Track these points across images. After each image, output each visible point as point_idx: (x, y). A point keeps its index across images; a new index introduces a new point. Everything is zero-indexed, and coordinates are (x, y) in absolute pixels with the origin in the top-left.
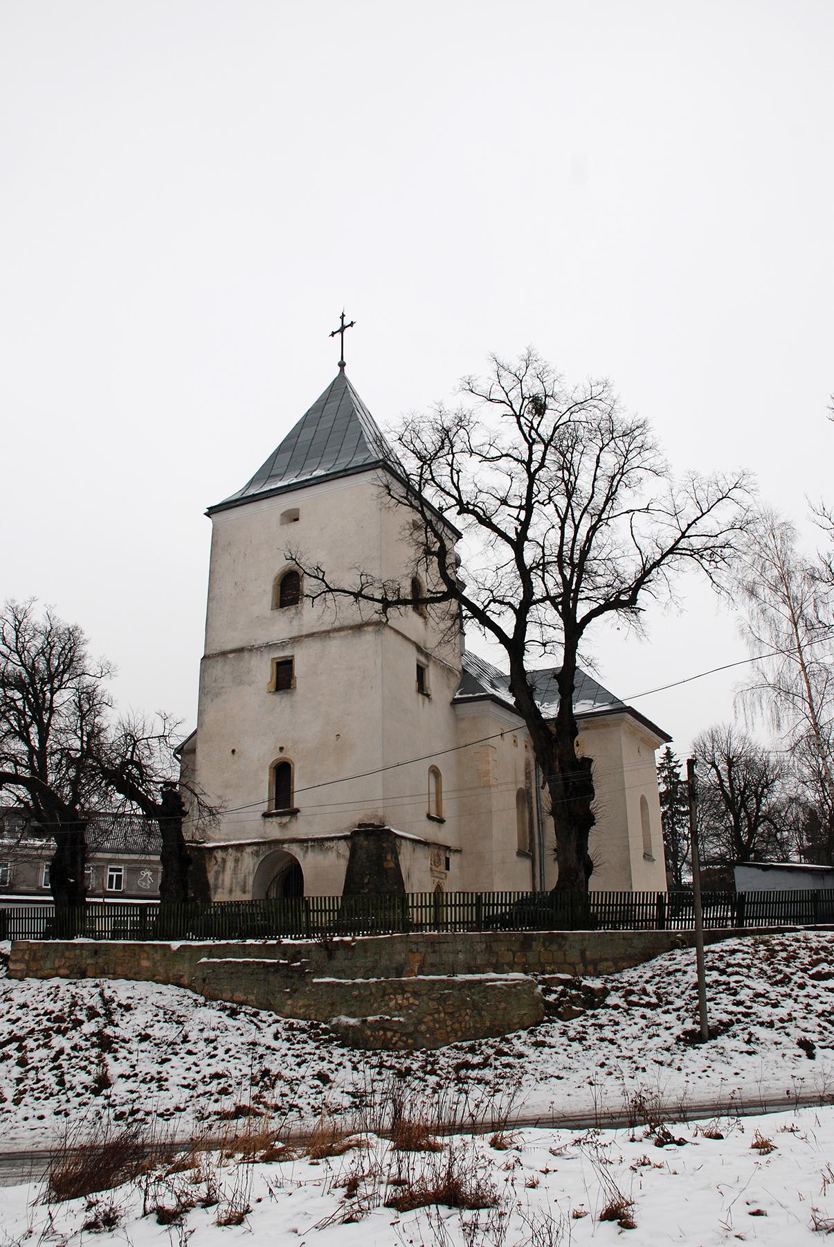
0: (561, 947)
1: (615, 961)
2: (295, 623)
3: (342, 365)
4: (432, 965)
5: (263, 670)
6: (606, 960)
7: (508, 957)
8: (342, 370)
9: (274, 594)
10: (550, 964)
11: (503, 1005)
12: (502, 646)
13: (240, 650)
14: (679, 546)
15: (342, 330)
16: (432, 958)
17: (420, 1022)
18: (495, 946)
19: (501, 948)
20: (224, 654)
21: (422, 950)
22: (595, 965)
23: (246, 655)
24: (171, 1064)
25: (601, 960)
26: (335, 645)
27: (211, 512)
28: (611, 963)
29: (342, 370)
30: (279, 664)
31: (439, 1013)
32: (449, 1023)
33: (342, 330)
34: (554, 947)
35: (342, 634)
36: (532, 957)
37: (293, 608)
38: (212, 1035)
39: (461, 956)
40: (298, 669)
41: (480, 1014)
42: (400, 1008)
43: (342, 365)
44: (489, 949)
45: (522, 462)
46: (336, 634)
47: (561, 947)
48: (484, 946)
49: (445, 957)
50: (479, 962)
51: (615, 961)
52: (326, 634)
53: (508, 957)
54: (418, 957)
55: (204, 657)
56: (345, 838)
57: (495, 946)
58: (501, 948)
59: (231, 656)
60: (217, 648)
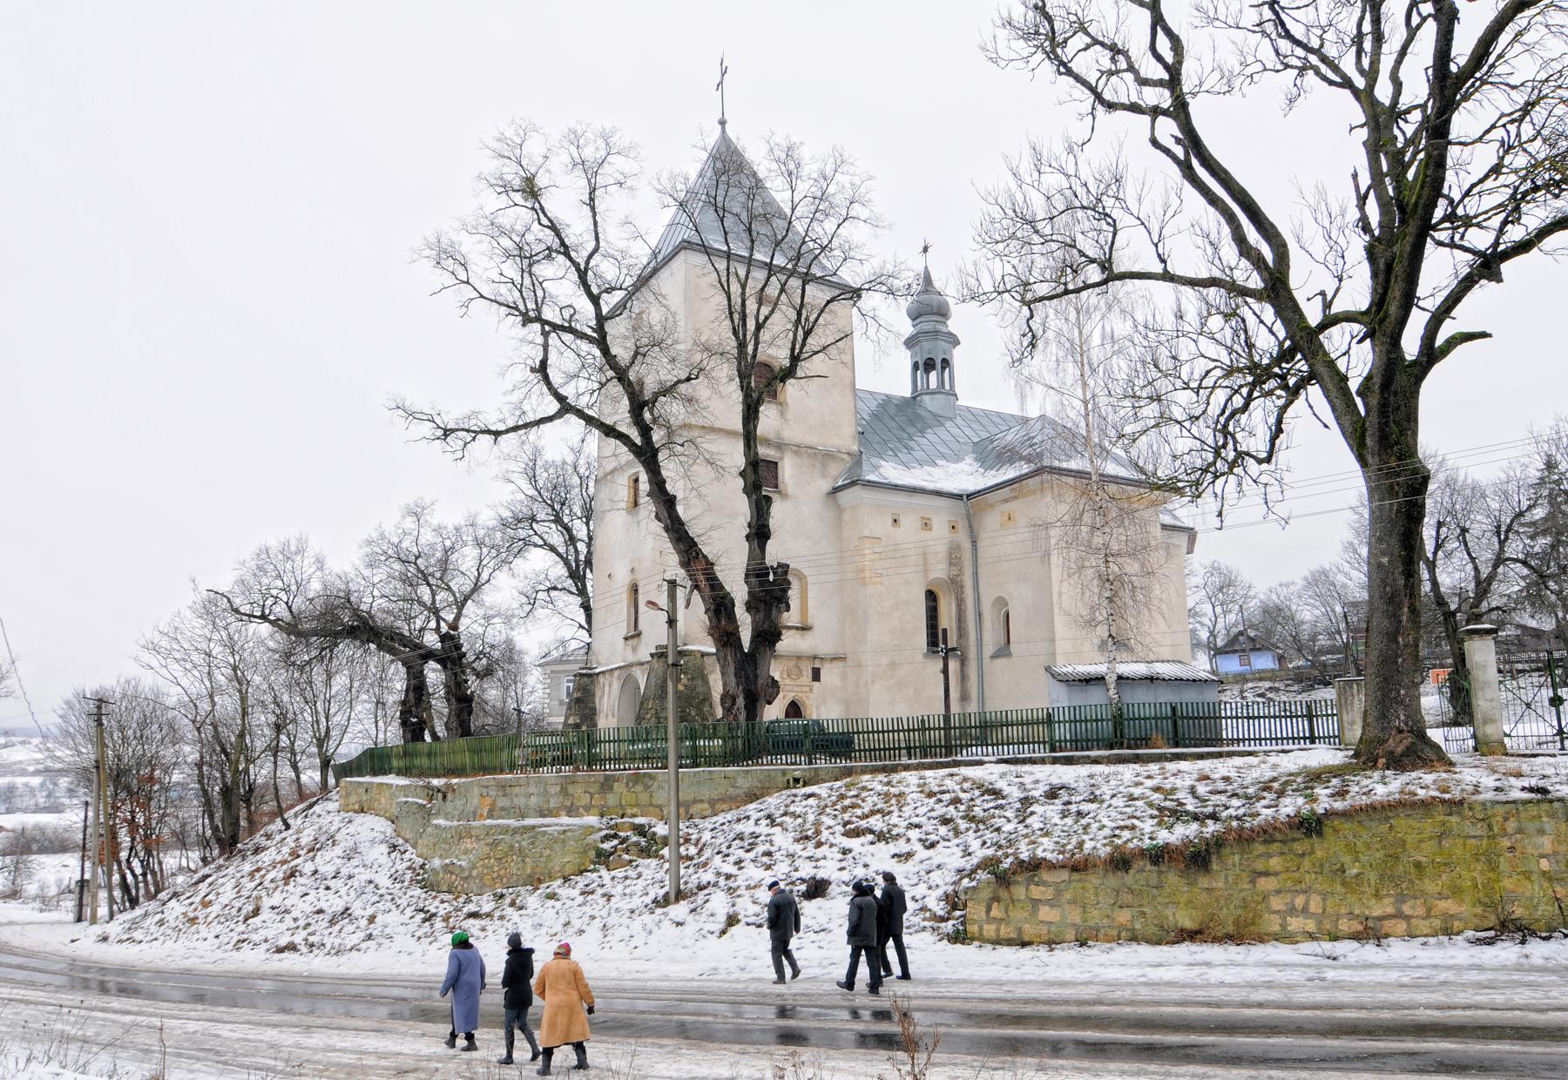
0: (647, 787)
1: (712, 803)
3: (723, 123)
4: (502, 809)
6: (702, 801)
7: (586, 799)
8: (724, 131)
10: (632, 806)
11: (547, 852)
14: (429, 603)
16: (502, 802)
17: (474, 867)
18: (571, 789)
19: (577, 790)
21: (493, 793)
22: (687, 808)
24: (829, 937)
25: (695, 802)
28: (706, 805)
29: (724, 131)
34: (639, 788)
36: (612, 799)
39: (533, 799)
42: (466, 852)
43: (723, 123)
44: (564, 791)
45: (1087, 47)
47: (647, 787)
48: (558, 788)
49: (516, 800)
50: (552, 805)
51: (712, 803)
53: (586, 799)
54: (488, 801)
57: (571, 789)
58: (577, 790)
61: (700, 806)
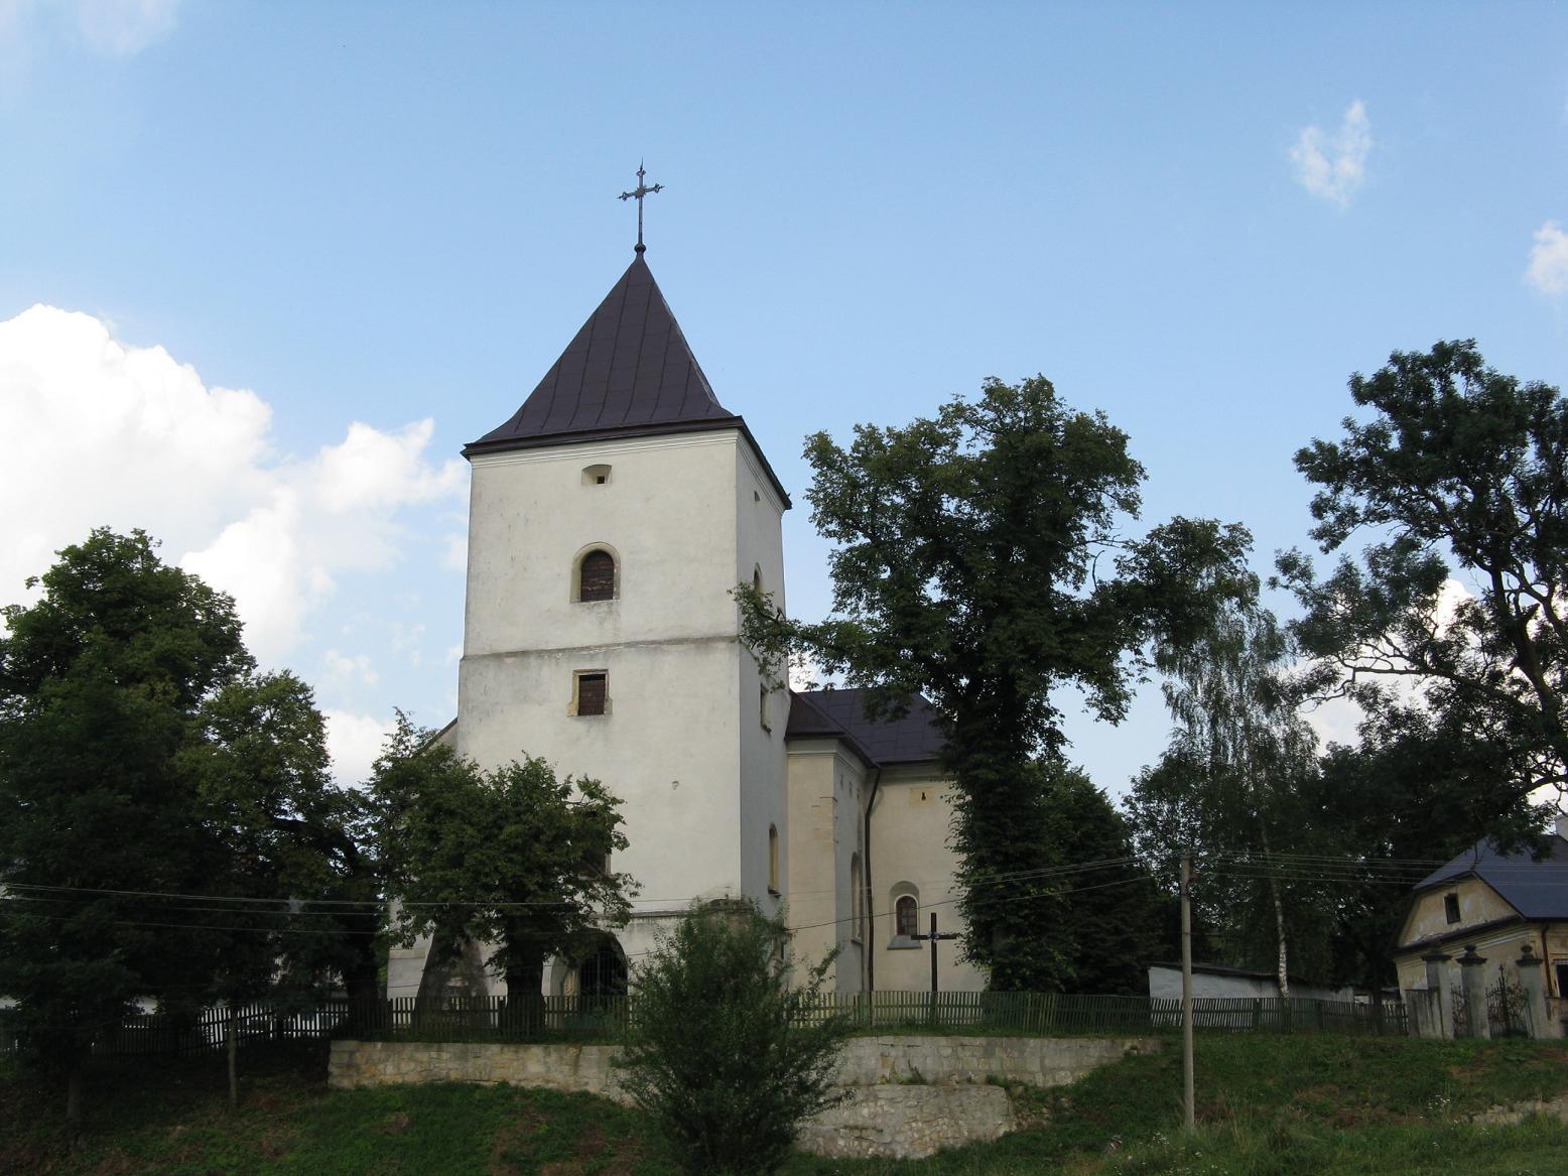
2: (608, 625)
3: (640, 249)
5: (563, 689)
6: (1062, 1069)
9: (573, 578)
12: (23, 314)
13: (524, 653)
15: (640, 193)
20: (498, 656)
23: (533, 661)
26: (671, 663)
27: (472, 451)
30: (582, 679)
31: (916, 1121)
32: (927, 1132)
33: (640, 193)
35: (681, 648)
37: (604, 604)
38: (1522, 1059)
40: (615, 688)
41: (957, 1124)
43: (640, 249)
46: (674, 648)
52: (655, 645)
55: (464, 659)
56: (678, 915)
59: (509, 661)
60: (483, 647)
61: (1063, 1073)
